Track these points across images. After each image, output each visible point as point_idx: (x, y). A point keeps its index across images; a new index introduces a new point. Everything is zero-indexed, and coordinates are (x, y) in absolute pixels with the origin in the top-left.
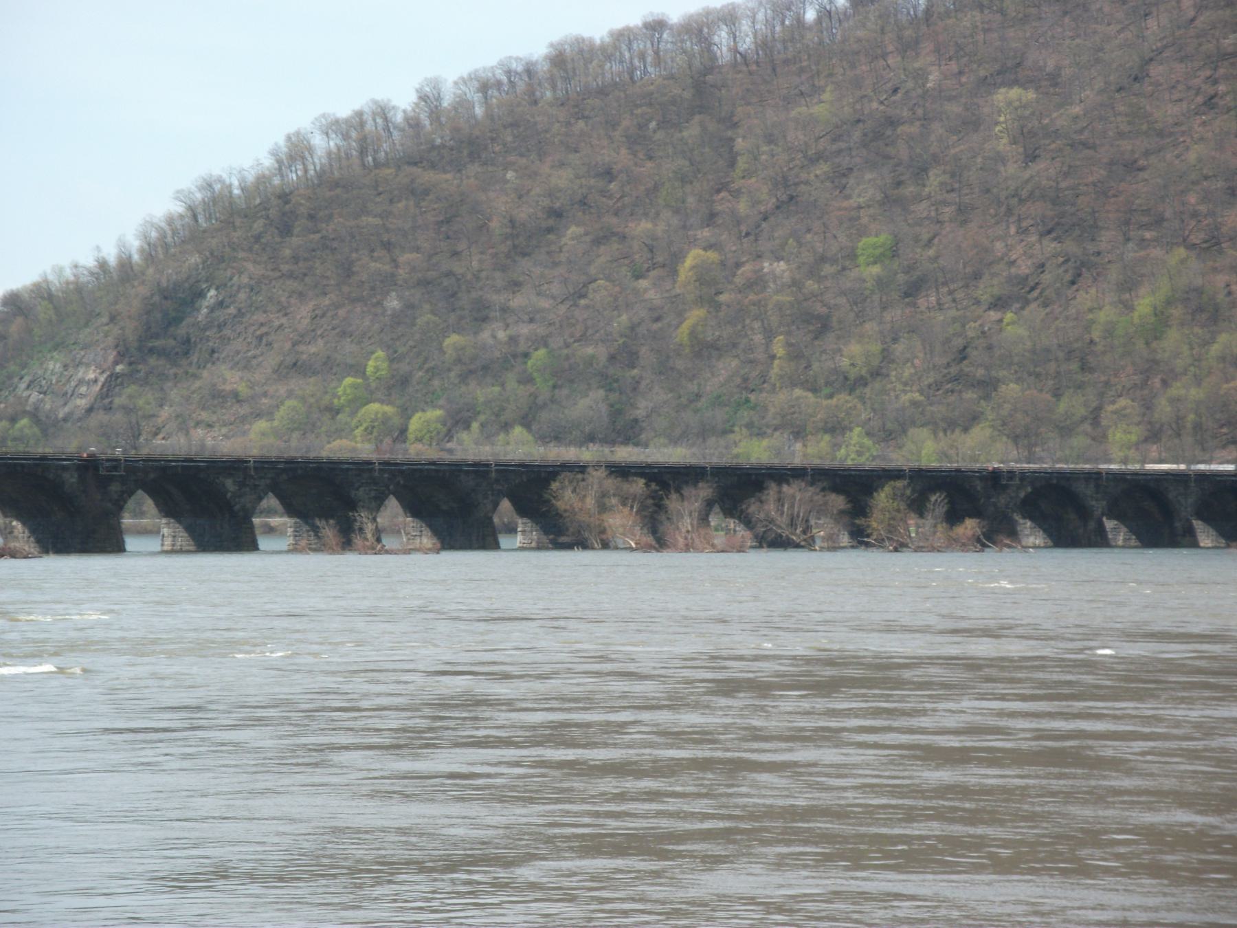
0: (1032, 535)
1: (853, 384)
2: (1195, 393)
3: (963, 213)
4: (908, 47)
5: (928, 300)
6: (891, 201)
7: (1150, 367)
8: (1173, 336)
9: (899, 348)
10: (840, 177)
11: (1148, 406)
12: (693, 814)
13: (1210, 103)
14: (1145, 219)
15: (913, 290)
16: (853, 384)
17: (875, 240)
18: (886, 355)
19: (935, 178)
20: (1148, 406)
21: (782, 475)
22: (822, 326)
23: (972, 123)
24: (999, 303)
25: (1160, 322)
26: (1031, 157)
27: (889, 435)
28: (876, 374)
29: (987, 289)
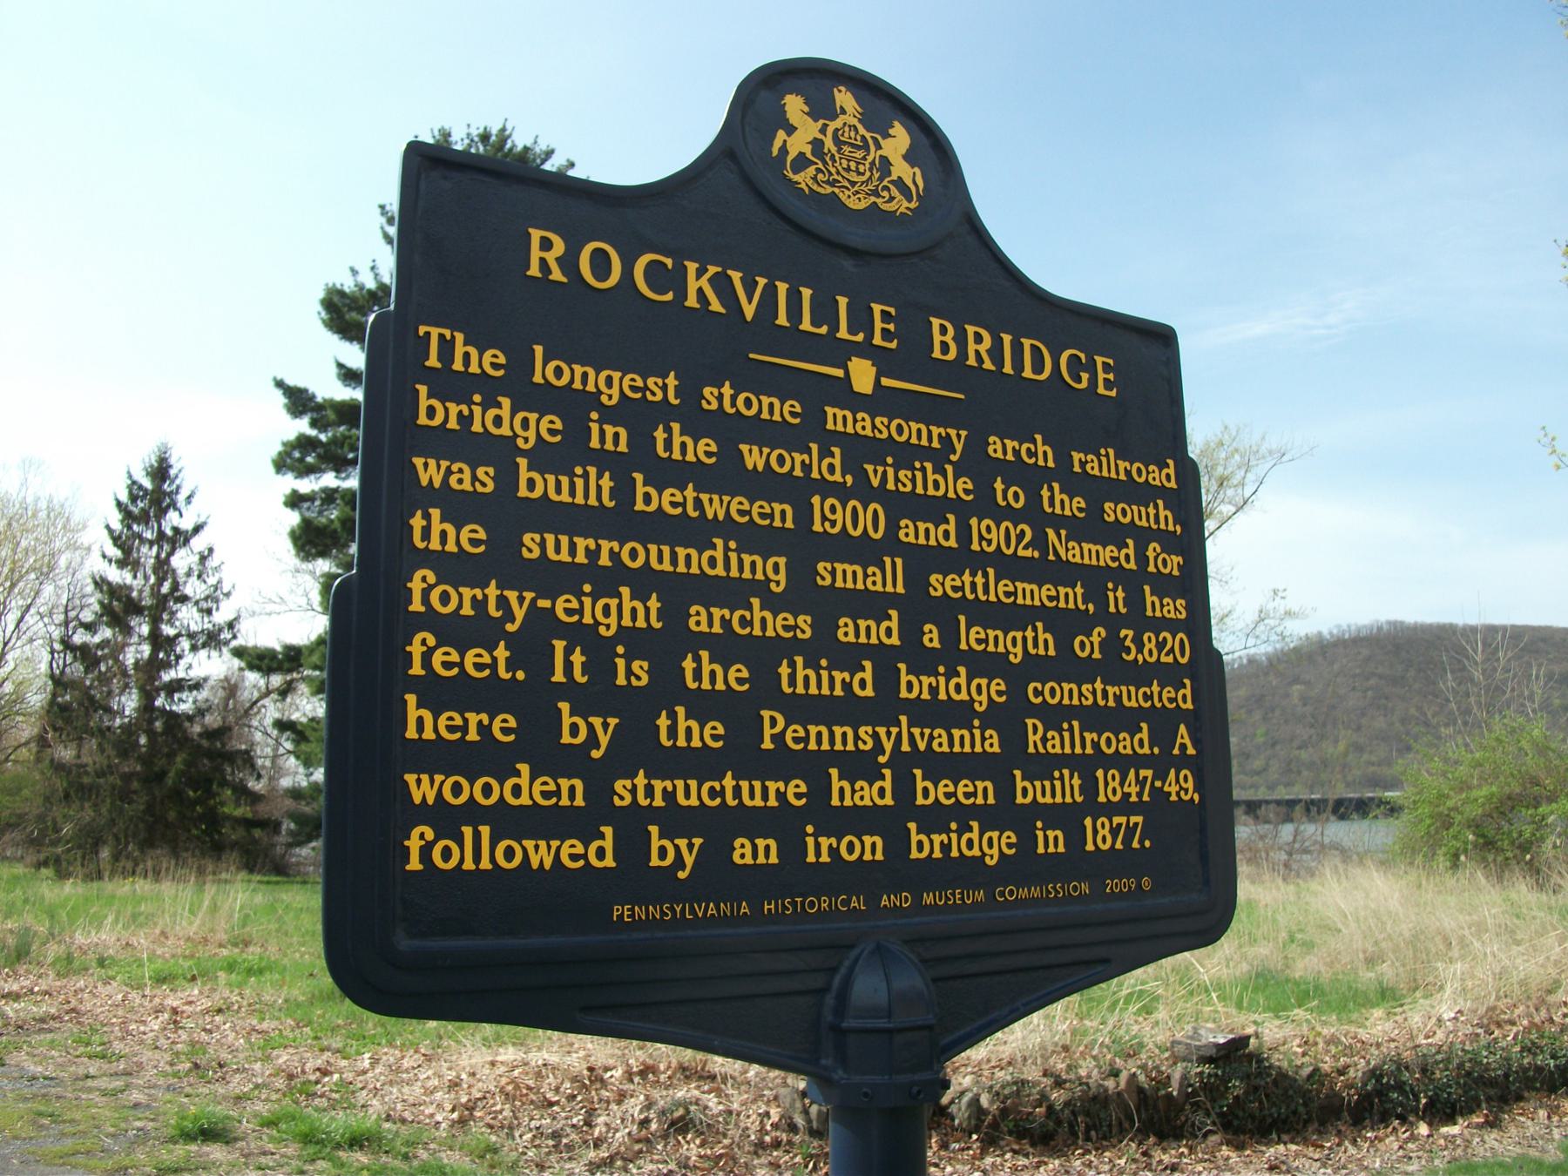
0: (1355, 816)
1: (1258, 773)
2: (1359, 773)
3: (1286, 722)
4: (1266, 674)
5: (1278, 747)
6: (1265, 719)
7: (1344, 766)
8: (1351, 757)
9: (1271, 762)
10: (1250, 712)
11: (1345, 777)
12: (1442, 1111)
13: (1354, 688)
14: (263, 1160)
15: (1274, 744)
16: (1258, 773)
17: (1261, 731)
18: (1267, 764)
19: (1278, 712)
20: (1345, 777)
21: (1267, 802)
22: (1248, 756)
23: (1287, 695)
24: (1299, 748)
25: (1346, 754)
26: (1305, 705)
27: (1271, 787)
28: (1265, 770)
29: (1295, 744)
